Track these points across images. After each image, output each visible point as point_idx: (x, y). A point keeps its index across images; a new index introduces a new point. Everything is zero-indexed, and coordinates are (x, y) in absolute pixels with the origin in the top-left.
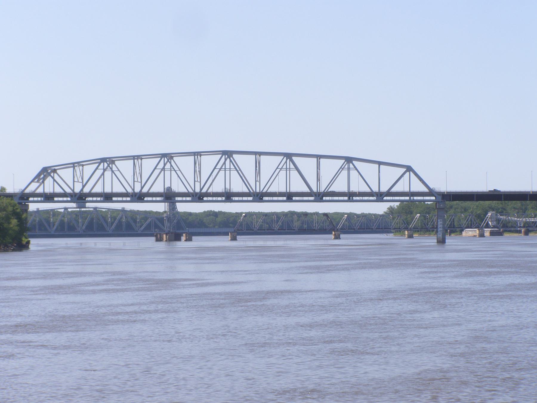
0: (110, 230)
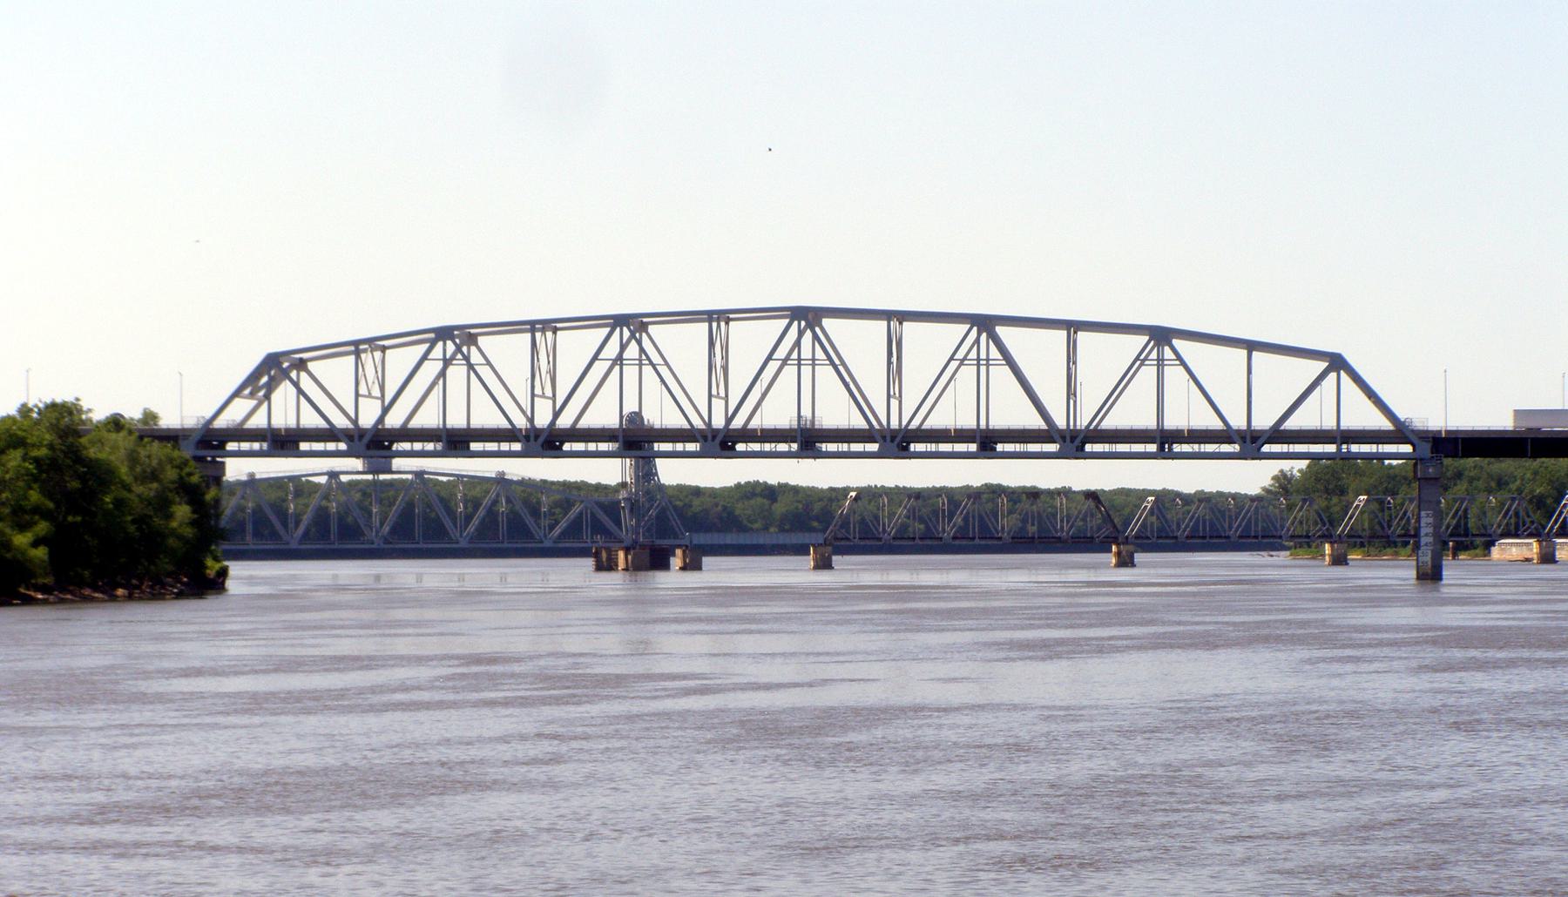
0: (461, 536)
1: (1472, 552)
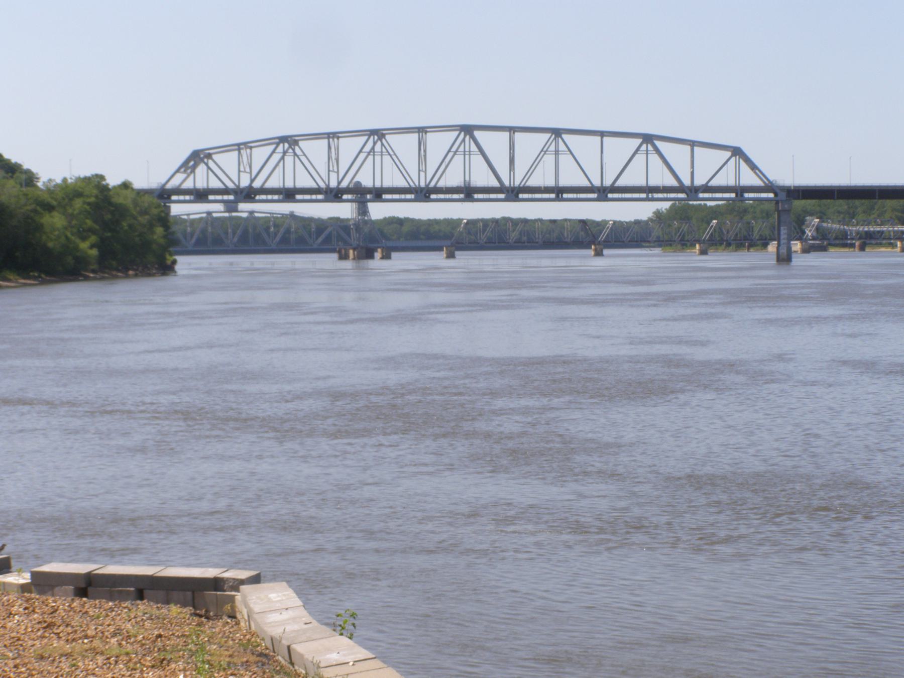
0: (272, 242)
1: (755, 248)
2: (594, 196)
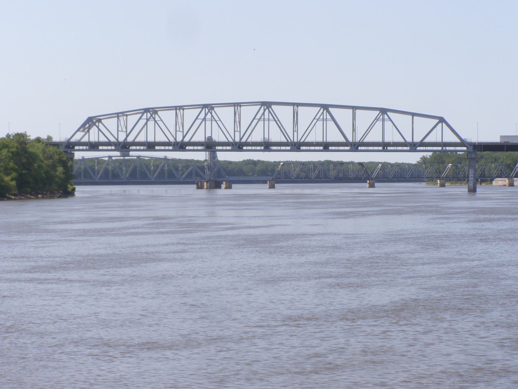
0: (152, 177)
1: (486, 183)
2: (408, 148)
